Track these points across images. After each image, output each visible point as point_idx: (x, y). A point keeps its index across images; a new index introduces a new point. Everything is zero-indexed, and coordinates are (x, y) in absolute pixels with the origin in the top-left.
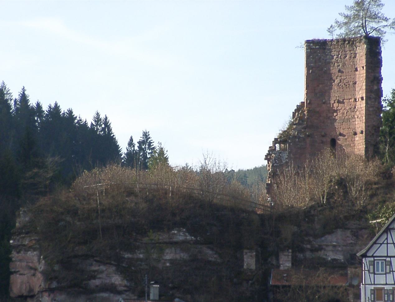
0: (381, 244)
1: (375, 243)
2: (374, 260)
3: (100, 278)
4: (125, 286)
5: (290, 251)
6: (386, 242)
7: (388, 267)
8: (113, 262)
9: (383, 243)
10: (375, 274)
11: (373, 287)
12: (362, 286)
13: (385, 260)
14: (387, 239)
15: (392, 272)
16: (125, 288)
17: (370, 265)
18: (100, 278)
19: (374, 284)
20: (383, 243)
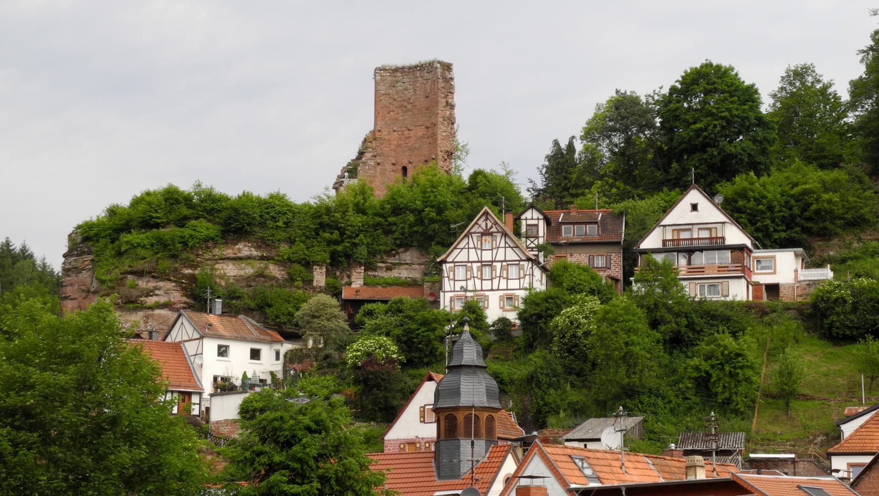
0: (462, 249)
1: (455, 248)
2: (455, 266)
3: (157, 295)
4: (186, 303)
5: (363, 268)
6: (467, 247)
7: (469, 273)
8: (172, 278)
9: (464, 248)
10: (455, 280)
11: (452, 294)
12: (442, 294)
13: (466, 266)
14: (468, 243)
15: (494, 264)
16: (185, 305)
17: (450, 271)
18: (157, 295)
19: (454, 291)
20: (464, 248)
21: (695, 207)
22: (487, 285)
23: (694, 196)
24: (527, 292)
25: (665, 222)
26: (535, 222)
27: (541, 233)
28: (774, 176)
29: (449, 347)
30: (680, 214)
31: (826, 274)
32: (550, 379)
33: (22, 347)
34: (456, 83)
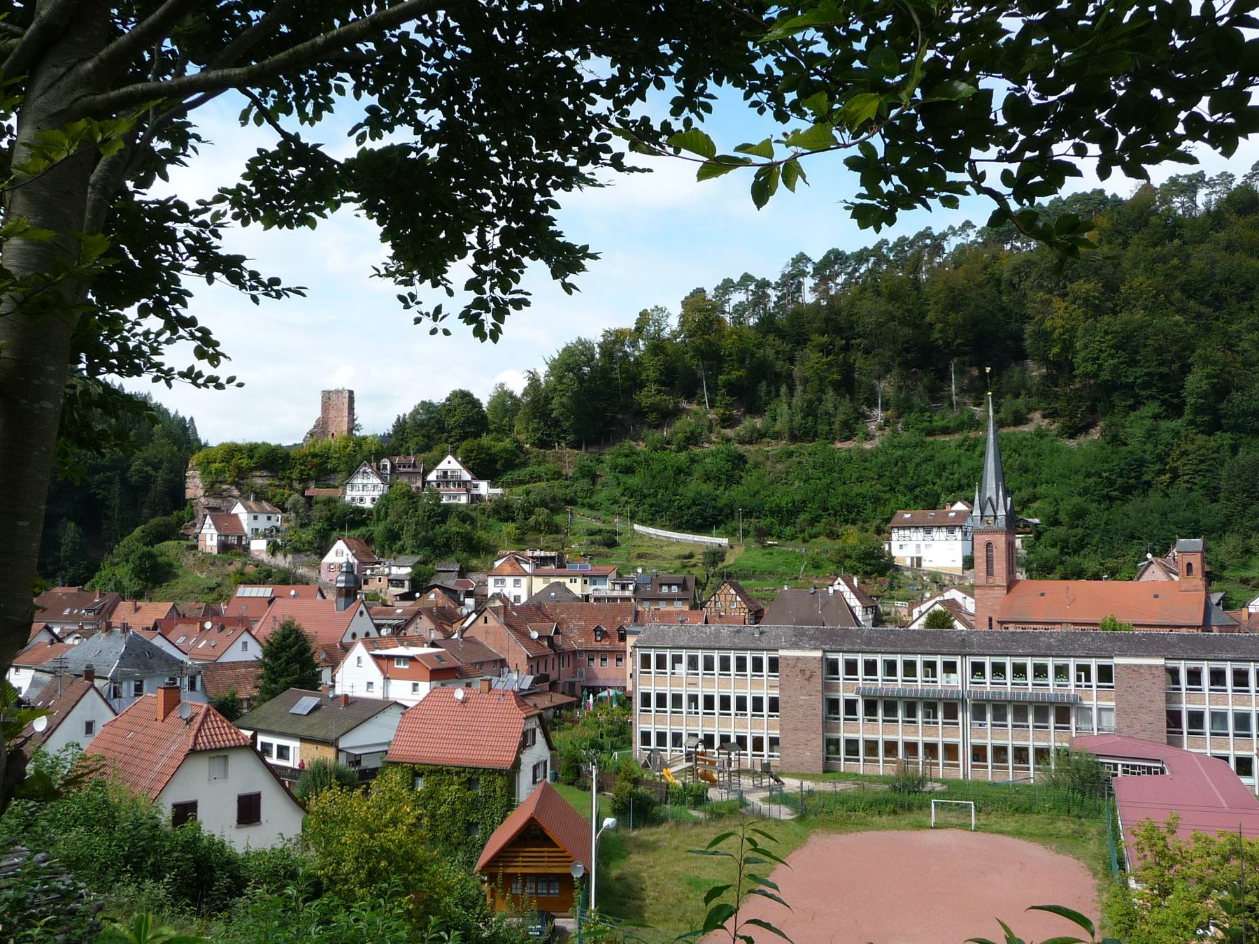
22: (365, 493)
23: (450, 458)
30: (443, 465)
31: (499, 491)
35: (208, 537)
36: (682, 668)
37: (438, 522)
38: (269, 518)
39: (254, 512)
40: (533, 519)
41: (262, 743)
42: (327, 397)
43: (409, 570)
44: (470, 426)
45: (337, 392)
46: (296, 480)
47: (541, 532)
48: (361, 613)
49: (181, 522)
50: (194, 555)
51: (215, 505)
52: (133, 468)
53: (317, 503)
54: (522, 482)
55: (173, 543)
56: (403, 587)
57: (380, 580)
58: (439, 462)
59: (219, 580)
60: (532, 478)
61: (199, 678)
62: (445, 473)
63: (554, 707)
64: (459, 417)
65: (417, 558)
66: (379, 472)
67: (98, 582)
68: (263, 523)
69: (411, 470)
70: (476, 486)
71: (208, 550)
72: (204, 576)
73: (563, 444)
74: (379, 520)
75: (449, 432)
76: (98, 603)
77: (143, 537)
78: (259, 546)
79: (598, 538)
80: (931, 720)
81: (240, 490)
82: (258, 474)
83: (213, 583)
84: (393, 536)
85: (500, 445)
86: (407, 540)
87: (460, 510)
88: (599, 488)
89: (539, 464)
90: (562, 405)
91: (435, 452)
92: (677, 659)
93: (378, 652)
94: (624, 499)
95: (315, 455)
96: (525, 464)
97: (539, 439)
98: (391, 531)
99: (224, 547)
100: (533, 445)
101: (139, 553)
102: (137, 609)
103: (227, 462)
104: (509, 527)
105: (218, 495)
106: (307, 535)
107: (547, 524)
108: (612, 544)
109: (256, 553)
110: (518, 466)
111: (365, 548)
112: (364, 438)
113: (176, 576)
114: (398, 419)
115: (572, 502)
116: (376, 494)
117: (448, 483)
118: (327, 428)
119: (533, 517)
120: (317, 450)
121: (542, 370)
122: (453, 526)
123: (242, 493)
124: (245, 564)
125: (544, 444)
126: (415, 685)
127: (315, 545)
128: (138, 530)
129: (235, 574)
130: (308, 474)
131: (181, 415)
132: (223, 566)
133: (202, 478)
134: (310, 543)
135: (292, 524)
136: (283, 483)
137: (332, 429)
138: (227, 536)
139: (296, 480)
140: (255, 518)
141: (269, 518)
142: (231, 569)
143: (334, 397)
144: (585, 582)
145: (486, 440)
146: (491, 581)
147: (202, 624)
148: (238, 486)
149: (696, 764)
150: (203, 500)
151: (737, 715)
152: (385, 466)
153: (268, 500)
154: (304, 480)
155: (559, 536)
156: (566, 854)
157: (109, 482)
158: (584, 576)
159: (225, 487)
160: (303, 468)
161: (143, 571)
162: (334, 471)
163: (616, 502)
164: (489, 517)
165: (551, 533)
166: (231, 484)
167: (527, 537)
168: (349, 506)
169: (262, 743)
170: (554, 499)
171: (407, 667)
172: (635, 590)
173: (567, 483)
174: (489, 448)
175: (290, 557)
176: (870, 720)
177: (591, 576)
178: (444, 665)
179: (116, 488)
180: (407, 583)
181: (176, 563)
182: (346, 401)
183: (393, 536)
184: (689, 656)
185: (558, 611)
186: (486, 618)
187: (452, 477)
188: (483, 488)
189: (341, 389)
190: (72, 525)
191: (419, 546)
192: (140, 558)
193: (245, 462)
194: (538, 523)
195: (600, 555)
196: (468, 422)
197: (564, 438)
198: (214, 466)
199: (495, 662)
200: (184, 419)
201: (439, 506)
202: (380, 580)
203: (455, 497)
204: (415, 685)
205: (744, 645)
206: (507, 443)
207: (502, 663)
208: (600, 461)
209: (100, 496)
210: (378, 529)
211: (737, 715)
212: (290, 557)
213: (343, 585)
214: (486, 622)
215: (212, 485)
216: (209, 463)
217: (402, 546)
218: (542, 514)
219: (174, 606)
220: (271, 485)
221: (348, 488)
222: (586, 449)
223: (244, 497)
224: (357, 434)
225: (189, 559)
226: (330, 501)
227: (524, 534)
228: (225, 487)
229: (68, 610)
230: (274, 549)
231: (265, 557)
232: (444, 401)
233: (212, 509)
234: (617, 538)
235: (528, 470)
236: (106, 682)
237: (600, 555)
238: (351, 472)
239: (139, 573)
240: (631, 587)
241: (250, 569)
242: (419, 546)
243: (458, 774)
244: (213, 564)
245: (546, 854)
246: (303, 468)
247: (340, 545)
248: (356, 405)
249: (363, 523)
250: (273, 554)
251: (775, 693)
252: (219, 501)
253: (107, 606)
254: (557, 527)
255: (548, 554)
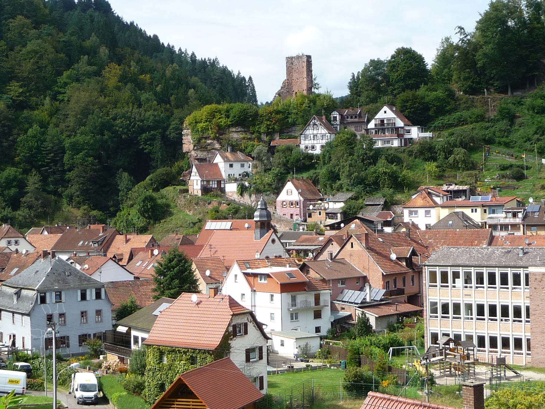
21: (385, 112)
22: (315, 142)
23: (385, 108)
24: (22, 348)
25: (376, 117)
26: (336, 115)
27: (338, 119)
28: (232, 205)
29: (317, 201)
30: (380, 115)
31: (428, 134)
32: (57, 86)
33: (159, 179)
34: (313, 62)
35: (195, 182)
36: (460, 282)
37: (370, 164)
38: (243, 166)
39: (229, 161)
40: (451, 159)
41: (134, 336)
42: (290, 61)
43: (342, 205)
44: (410, 78)
45: (298, 57)
46: (264, 133)
47: (459, 169)
48: (273, 241)
49: (180, 171)
50: (184, 197)
51: (202, 156)
52: (171, 127)
53: (278, 151)
54: (450, 126)
55: (170, 188)
56: (337, 219)
57: (320, 214)
58: (376, 113)
59: (200, 216)
60: (460, 121)
61: (103, 290)
62: (382, 121)
63: (397, 314)
64: (401, 72)
65: (350, 195)
66: (329, 125)
67: (118, 220)
68: (237, 170)
69: (356, 120)
70: (409, 131)
71: (195, 193)
72: (191, 213)
73: (492, 90)
74: (324, 164)
75: (393, 86)
76: (101, 236)
77: (152, 184)
78: (231, 188)
79: (508, 172)
80: (470, 316)
81: (220, 143)
82: (234, 129)
83: (195, 219)
84: (334, 177)
85: (433, 95)
86: (344, 180)
87: (390, 152)
88: (516, 127)
89: (468, 108)
90: (485, 55)
91: (379, 104)
92: (456, 275)
93: (249, 271)
94: (536, 136)
95: (278, 112)
96: (455, 110)
97: (470, 87)
98: (331, 172)
99: (205, 190)
100: (465, 92)
101: (143, 197)
102: (127, 241)
103: (210, 122)
104: (431, 166)
105: (204, 148)
106: (268, 178)
107: (464, 162)
108: (520, 177)
109: (230, 194)
110: (450, 112)
111: (312, 187)
112: (319, 95)
113: (171, 214)
114: (354, 77)
115: (489, 142)
116: (324, 142)
117: (383, 130)
118: (291, 89)
119: (453, 156)
120: (280, 108)
121: (471, 27)
122: (382, 166)
123: (222, 146)
124: (220, 203)
125: (473, 91)
126: (272, 296)
127: (273, 186)
128: (148, 178)
129: (212, 211)
130: (273, 128)
131: (242, 75)
132: (204, 205)
133: (192, 135)
134: (270, 185)
135: (259, 169)
136: (253, 136)
137: (295, 89)
138: (208, 181)
139: (264, 133)
140: (231, 166)
141: (243, 166)
142: (210, 207)
143: (296, 62)
144: (485, 211)
145: (422, 91)
146: (406, 212)
147: (152, 251)
148: (218, 140)
149: (446, 357)
150: (193, 153)
151: (502, 320)
152: (335, 118)
153: (241, 151)
154: (270, 133)
155: (474, 172)
156: (203, 404)
157: (153, 138)
158: (483, 206)
159: (209, 141)
160: (268, 123)
161: (146, 211)
162: (294, 124)
163: (529, 139)
164: (415, 158)
165: (468, 170)
166: (213, 139)
167: (447, 174)
168: (301, 153)
169: (134, 336)
170: (472, 139)
171: (266, 282)
172: (524, 218)
173: (487, 124)
174: (423, 98)
175: (253, 197)
176: (492, 320)
177: (490, 206)
178: (293, 280)
179: (158, 143)
180: (339, 215)
181: (172, 204)
182: (305, 64)
183: (334, 177)
184: (453, 272)
185: (427, 237)
186: (352, 243)
187: (388, 124)
188: (415, 133)
189: (301, 54)
190: (126, 175)
191: (352, 185)
192: (144, 201)
193: (223, 121)
194: (456, 162)
195: (508, 187)
196: (409, 75)
197: (492, 85)
198: (200, 125)
199: (358, 278)
200: (244, 79)
201: (371, 150)
202: (320, 214)
203: (388, 142)
204: (272, 296)
205: (507, 264)
206: (440, 93)
207: (365, 279)
208: (520, 103)
209: (147, 150)
210: (322, 171)
211: (502, 320)
212: (253, 197)
213: (258, 219)
214: (352, 247)
215: (199, 140)
216: (196, 122)
217: (341, 185)
218: (459, 153)
219: (152, 238)
220: (244, 138)
221: (302, 137)
222: (512, 93)
223: (223, 149)
224: (316, 91)
225: (181, 201)
226: (289, 149)
227: (444, 171)
228: (209, 141)
229: (81, 243)
230: (242, 190)
231: (236, 197)
232: (389, 58)
233: (201, 160)
234: (525, 172)
235: (457, 115)
236: (313, 304)
237: (508, 187)
238: (306, 124)
239: (143, 212)
240: (520, 215)
241: (224, 207)
242: (352, 185)
243: (185, 353)
244: (197, 204)
245: (191, 403)
246: (268, 123)
247: (289, 186)
248: (313, 68)
249: (312, 166)
250: (241, 195)
251: (528, 302)
252: (205, 153)
253: (107, 239)
254: (473, 163)
255: (461, 188)
